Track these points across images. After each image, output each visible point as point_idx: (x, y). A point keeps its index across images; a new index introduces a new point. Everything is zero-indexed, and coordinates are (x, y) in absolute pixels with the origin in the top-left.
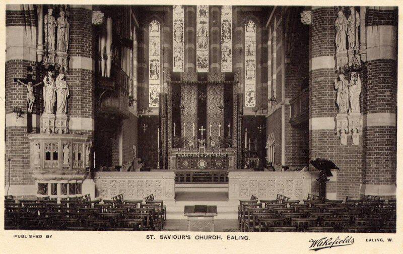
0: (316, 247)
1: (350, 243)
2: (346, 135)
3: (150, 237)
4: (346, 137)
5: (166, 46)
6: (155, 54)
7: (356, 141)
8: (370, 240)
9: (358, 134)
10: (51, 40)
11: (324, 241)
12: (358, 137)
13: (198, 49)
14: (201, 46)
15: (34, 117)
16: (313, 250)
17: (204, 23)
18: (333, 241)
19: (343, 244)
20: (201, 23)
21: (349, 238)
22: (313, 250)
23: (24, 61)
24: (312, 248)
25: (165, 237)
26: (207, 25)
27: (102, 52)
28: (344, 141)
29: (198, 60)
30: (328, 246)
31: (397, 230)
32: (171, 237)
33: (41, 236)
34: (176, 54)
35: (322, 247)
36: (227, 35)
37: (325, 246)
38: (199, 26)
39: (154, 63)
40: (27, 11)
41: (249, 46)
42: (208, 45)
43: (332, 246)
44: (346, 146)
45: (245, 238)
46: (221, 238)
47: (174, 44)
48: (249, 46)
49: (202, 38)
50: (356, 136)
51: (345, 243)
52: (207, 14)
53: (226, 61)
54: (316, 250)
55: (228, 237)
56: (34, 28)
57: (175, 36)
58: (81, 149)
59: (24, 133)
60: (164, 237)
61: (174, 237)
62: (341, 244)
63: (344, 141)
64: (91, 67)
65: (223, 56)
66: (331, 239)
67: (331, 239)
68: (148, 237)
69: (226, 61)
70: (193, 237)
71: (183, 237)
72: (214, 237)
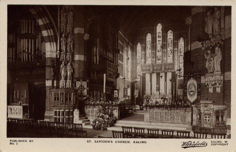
0: (185, 146)
1: (205, 145)
2: (212, 87)
3: (89, 141)
4: (212, 88)
5: (143, 52)
6: (139, 57)
7: (218, 90)
8: (137, 142)
9: (220, 86)
10: (64, 48)
11: (190, 143)
12: (220, 87)
13: (157, 52)
14: (158, 51)
15: (55, 82)
16: (183, 147)
17: (160, 41)
18: (195, 143)
19: (200, 146)
20: (159, 41)
21: (204, 143)
22: (183, 147)
23: (50, 58)
24: (183, 146)
25: (98, 142)
26: (161, 41)
27: (95, 53)
28: (211, 90)
29: (157, 57)
30: (192, 146)
31: (8, 138)
32: (101, 141)
33: (26, 141)
34: (147, 55)
35: (188, 146)
36: (170, 45)
37: (190, 146)
38: (158, 42)
39: (139, 60)
40: (50, 36)
41: (181, 49)
42: (161, 50)
43: (194, 146)
44: (212, 93)
45: (145, 142)
46: (130, 142)
47: (147, 51)
48: (181, 49)
49: (159, 47)
50: (218, 87)
51: (202, 145)
52: (161, 37)
53: (170, 56)
54: (185, 148)
55: (134, 142)
56: (55, 43)
57: (147, 48)
58: (71, 95)
59: (50, 89)
60: (97, 142)
61: (102, 142)
62: (200, 145)
63: (211, 90)
64: (49, 56)
65: (168, 54)
66: (194, 142)
67: (194, 142)
68: (88, 142)
69: (170, 56)
70: (114, 141)
71: (109, 142)
72: (126, 142)
